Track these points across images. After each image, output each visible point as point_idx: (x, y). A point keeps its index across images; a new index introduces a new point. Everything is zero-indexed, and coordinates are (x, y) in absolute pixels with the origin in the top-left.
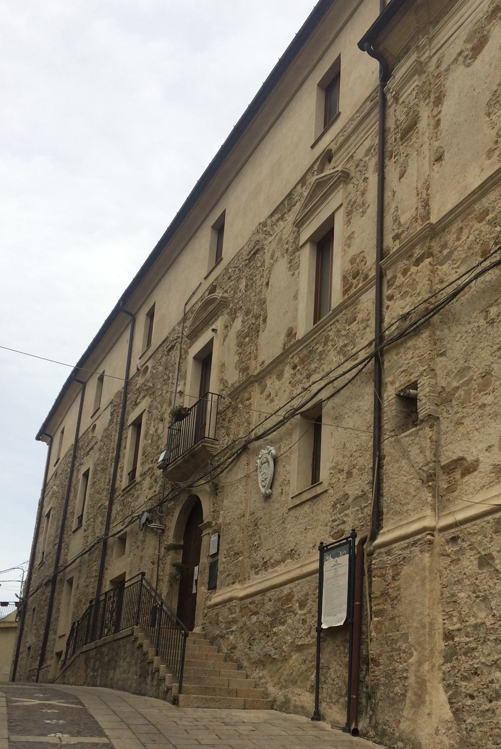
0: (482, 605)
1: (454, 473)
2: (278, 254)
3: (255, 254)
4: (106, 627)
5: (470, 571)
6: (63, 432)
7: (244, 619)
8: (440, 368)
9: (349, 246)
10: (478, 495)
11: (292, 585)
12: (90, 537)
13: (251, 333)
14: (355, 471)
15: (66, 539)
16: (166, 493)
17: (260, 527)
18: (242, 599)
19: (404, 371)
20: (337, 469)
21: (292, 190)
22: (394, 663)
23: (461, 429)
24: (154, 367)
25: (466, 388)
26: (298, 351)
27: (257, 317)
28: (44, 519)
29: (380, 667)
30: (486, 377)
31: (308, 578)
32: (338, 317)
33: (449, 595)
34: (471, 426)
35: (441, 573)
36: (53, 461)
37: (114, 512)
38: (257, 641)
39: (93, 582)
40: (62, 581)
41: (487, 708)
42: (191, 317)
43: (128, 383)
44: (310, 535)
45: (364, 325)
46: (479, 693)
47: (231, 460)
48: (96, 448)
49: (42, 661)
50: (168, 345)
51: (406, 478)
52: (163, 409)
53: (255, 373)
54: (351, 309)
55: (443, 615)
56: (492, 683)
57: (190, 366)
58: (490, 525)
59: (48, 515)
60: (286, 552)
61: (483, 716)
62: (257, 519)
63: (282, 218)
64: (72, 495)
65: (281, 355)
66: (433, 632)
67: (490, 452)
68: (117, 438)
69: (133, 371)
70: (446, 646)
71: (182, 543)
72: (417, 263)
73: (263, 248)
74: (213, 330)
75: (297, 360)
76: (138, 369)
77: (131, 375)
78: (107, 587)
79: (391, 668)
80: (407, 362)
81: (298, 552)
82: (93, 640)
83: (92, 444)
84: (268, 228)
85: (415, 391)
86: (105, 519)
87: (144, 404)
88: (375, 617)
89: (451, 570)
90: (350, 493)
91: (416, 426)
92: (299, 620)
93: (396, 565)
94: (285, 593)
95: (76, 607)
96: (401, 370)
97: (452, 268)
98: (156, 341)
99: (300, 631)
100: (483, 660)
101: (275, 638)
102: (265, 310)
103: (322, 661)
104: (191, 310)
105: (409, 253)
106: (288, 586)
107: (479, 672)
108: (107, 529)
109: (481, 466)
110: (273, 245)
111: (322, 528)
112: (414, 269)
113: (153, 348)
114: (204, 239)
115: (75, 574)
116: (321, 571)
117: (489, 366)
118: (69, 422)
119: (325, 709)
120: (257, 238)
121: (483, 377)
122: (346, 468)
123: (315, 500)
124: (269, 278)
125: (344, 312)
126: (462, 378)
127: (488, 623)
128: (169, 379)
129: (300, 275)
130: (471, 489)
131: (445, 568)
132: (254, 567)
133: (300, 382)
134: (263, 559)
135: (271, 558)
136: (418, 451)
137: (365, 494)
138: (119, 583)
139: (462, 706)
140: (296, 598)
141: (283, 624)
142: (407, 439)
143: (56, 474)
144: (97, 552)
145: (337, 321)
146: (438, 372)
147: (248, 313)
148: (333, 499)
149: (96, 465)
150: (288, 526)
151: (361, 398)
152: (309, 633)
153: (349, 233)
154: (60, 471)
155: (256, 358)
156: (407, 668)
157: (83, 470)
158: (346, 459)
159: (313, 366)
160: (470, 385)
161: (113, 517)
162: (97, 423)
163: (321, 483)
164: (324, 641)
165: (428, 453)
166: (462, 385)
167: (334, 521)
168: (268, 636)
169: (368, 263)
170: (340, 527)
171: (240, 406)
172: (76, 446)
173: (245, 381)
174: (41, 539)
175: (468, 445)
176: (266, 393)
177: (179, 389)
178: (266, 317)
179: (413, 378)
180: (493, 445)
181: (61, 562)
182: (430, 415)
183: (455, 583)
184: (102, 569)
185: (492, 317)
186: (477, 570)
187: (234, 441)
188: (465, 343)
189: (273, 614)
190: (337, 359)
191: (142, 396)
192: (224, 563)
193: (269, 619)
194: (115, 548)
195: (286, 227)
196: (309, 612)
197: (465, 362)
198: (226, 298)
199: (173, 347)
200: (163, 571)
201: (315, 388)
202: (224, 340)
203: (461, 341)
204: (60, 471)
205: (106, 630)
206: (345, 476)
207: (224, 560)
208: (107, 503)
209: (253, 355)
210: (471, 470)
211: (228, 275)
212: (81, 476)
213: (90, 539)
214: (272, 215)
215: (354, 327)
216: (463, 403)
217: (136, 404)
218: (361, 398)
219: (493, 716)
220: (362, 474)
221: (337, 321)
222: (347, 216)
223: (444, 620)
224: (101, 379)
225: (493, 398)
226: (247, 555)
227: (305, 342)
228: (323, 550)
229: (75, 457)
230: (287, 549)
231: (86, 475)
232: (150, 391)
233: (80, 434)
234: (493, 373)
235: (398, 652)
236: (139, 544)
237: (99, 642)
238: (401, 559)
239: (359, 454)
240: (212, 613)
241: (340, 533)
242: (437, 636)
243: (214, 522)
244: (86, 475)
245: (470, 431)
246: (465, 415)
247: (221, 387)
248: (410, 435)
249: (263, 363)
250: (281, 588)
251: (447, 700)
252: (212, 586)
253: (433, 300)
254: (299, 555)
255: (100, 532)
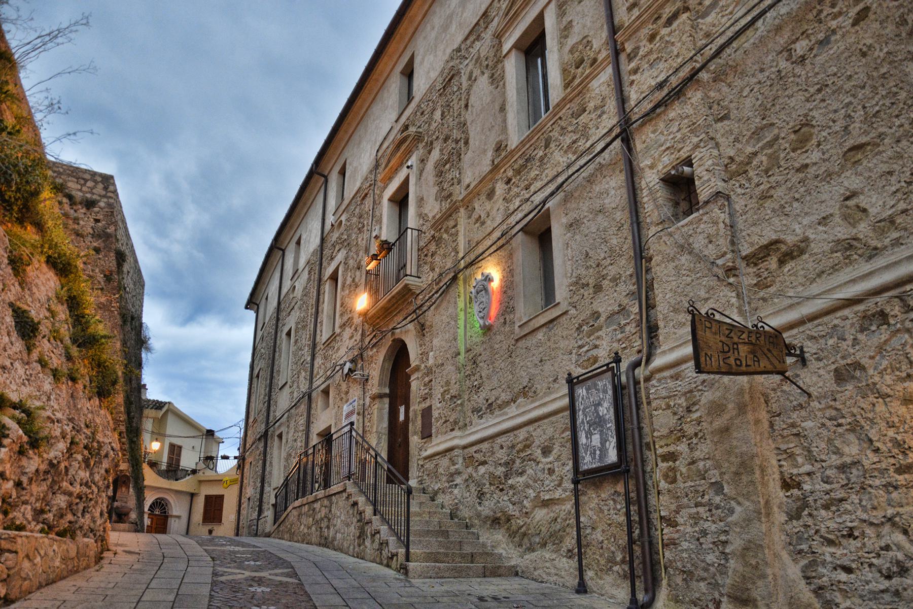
0: (851, 437)
1: (765, 263)
2: (477, 72)
3: (450, 80)
4: (317, 482)
5: (820, 390)
6: (267, 299)
7: (470, 470)
8: (723, 135)
9: (566, 37)
10: (815, 284)
11: (531, 428)
12: (295, 393)
13: (453, 159)
14: (605, 283)
15: (273, 397)
16: (367, 340)
17: (481, 364)
18: (465, 447)
19: (668, 148)
20: (578, 284)
21: (487, 9)
22: (702, 522)
23: (768, 204)
24: (348, 220)
25: (769, 151)
26: (511, 163)
27: (457, 141)
28: (255, 380)
29: (678, 528)
30: (802, 130)
31: (553, 419)
32: (560, 114)
33: (785, 426)
34: (787, 197)
35: (767, 396)
36: (260, 326)
37: (316, 366)
38: (488, 496)
39: (301, 436)
40: (272, 435)
41: (882, 587)
42: (383, 162)
43: (323, 240)
44: (547, 367)
45: (599, 112)
46: (862, 564)
47: (436, 296)
48: (296, 307)
49: (260, 512)
50: (362, 195)
51: (689, 279)
52: (360, 257)
53: (460, 198)
54: (578, 100)
55: (778, 455)
56: (887, 551)
57: (386, 209)
58: (848, 322)
59: (258, 376)
60: (516, 390)
61: (875, 599)
62: (475, 356)
63: (478, 38)
64: (277, 354)
65: (491, 171)
66: (766, 478)
67: (825, 225)
68: (315, 294)
69: (328, 227)
70: (787, 497)
71: (387, 391)
72: (669, 22)
73: (459, 73)
74: (408, 167)
75: (510, 173)
76: (332, 225)
77: (326, 231)
78: (314, 440)
79: (697, 529)
80: (672, 136)
81: (533, 389)
82: (304, 496)
83: (293, 304)
84: (463, 53)
85: (689, 169)
86: (308, 373)
87: (340, 257)
88: (663, 461)
89: (783, 391)
90: (600, 310)
91: (698, 210)
92: (544, 469)
93: (691, 391)
94: (521, 438)
95: (287, 460)
96: (663, 148)
97: (723, 16)
98: (349, 193)
99: (547, 482)
100: (865, 516)
101: (511, 493)
102: (466, 132)
103: (582, 519)
104: (383, 156)
105: (656, 16)
106: (525, 429)
107: (856, 534)
108: (311, 382)
109: (812, 245)
110: (470, 67)
111: (565, 357)
112: (664, 31)
113: (346, 202)
114: (394, 86)
115: (283, 429)
116: (572, 408)
117: (806, 115)
118: (272, 290)
119: (592, 579)
120: (451, 64)
121: (795, 132)
122: (592, 282)
123: (551, 326)
124: (468, 100)
125: (568, 106)
126: (759, 140)
127: (866, 463)
128: (363, 227)
129: (507, 84)
130: (801, 280)
131: (774, 390)
132: (476, 410)
133: (518, 195)
134: (487, 400)
135: (497, 399)
136: (706, 241)
137: (624, 309)
138: (327, 437)
139: (829, 583)
140: (537, 443)
141: (521, 474)
142: (686, 229)
143: (262, 338)
144: (303, 406)
145: (560, 118)
146: (721, 140)
147: (446, 140)
148: (576, 323)
149: (297, 323)
150: (517, 361)
151: (605, 195)
152: (560, 485)
153: (564, 23)
154: (266, 334)
155: (459, 182)
156: (727, 529)
157: (286, 330)
158: (591, 270)
159: (533, 174)
160: (775, 147)
161: (315, 372)
162: (296, 284)
163: (559, 303)
164: (584, 494)
165: (721, 241)
166: (762, 148)
167: (580, 347)
168: (502, 490)
169: (594, 46)
170: (589, 354)
171: (445, 236)
172: (278, 309)
173: (450, 208)
174: (253, 398)
175: (784, 222)
176: (475, 216)
177: (374, 234)
178: (468, 139)
179: (684, 154)
180: (831, 215)
181: (271, 418)
182: (720, 192)
183: (795, 409)
184: (308, 423)
185: (801, 53)
186: (835, 387)
187: (441, 275)
188: (760, 97)
189: (506, 464)
190: (565, 159)
191: (337, 249)
192: (438, 409)
193: (503, 469)
194: (319, 400)
195: (483, 47)
196: (558, 459)
197: (763, 119)
198: (421, 133)
199: (366, 195)
200: (370, 421)
201: (538, 198)
202: (421, 175)
203: (751, 95)
204: (266, 334)
205: (317, 485)
206: (591, 291)
207: (439, 405)
208: (309, 359)
209: (455, 180)
210: (795, 254)
211: (421, 111)
212: (284, 336)
213: (295, 395)
214: (466, 39)
215: (584, 118)
216: (766, 171)
217: (332, 259)
218: (605, 195)
219: (897, 600)
220: (617, 285)
221: (560, 118)
222: (560, 9)
223: (779, 461)
224: (298, 243)
225: (820, 154)
226: (466, 397)
227: (520, 150)
228: (572, 382)
229: (278, 319)
230: (517, 388)
231: (289, 334)
232: (345, 243)
233: (282, 297)
234: (814, 123)
235: (707, 508)
236: (343, 396)
237: (311, 498)
238: (699, 383)
239: (609, 261)
240: (429, 465)
241: (591, 361)
242: (771, 484)
243: (423, 366)
244: (289, 334)
245: (786, 203)
246: (774, 184)
247: (421, 222)
248: (691, 223)
249: (468, 186)
250: (515, 432)
251: (800, 574)
252: (427, 435)
253: (698, 58)
254: (535, 392)
255: (304, 387)
